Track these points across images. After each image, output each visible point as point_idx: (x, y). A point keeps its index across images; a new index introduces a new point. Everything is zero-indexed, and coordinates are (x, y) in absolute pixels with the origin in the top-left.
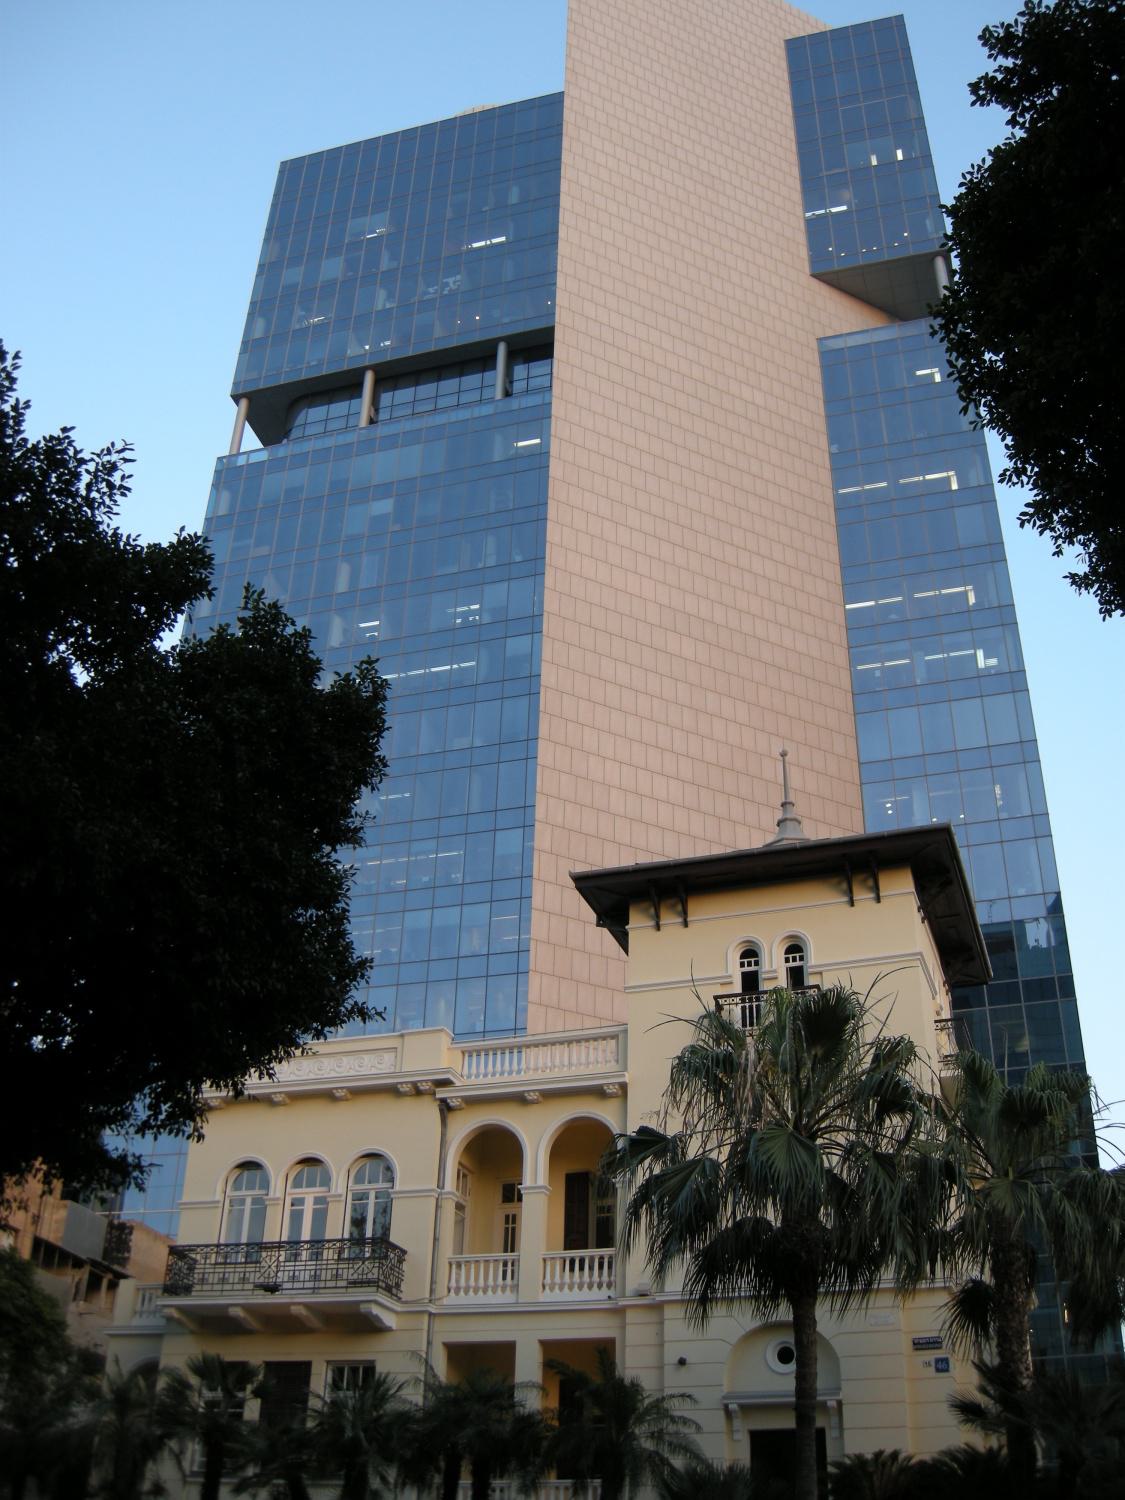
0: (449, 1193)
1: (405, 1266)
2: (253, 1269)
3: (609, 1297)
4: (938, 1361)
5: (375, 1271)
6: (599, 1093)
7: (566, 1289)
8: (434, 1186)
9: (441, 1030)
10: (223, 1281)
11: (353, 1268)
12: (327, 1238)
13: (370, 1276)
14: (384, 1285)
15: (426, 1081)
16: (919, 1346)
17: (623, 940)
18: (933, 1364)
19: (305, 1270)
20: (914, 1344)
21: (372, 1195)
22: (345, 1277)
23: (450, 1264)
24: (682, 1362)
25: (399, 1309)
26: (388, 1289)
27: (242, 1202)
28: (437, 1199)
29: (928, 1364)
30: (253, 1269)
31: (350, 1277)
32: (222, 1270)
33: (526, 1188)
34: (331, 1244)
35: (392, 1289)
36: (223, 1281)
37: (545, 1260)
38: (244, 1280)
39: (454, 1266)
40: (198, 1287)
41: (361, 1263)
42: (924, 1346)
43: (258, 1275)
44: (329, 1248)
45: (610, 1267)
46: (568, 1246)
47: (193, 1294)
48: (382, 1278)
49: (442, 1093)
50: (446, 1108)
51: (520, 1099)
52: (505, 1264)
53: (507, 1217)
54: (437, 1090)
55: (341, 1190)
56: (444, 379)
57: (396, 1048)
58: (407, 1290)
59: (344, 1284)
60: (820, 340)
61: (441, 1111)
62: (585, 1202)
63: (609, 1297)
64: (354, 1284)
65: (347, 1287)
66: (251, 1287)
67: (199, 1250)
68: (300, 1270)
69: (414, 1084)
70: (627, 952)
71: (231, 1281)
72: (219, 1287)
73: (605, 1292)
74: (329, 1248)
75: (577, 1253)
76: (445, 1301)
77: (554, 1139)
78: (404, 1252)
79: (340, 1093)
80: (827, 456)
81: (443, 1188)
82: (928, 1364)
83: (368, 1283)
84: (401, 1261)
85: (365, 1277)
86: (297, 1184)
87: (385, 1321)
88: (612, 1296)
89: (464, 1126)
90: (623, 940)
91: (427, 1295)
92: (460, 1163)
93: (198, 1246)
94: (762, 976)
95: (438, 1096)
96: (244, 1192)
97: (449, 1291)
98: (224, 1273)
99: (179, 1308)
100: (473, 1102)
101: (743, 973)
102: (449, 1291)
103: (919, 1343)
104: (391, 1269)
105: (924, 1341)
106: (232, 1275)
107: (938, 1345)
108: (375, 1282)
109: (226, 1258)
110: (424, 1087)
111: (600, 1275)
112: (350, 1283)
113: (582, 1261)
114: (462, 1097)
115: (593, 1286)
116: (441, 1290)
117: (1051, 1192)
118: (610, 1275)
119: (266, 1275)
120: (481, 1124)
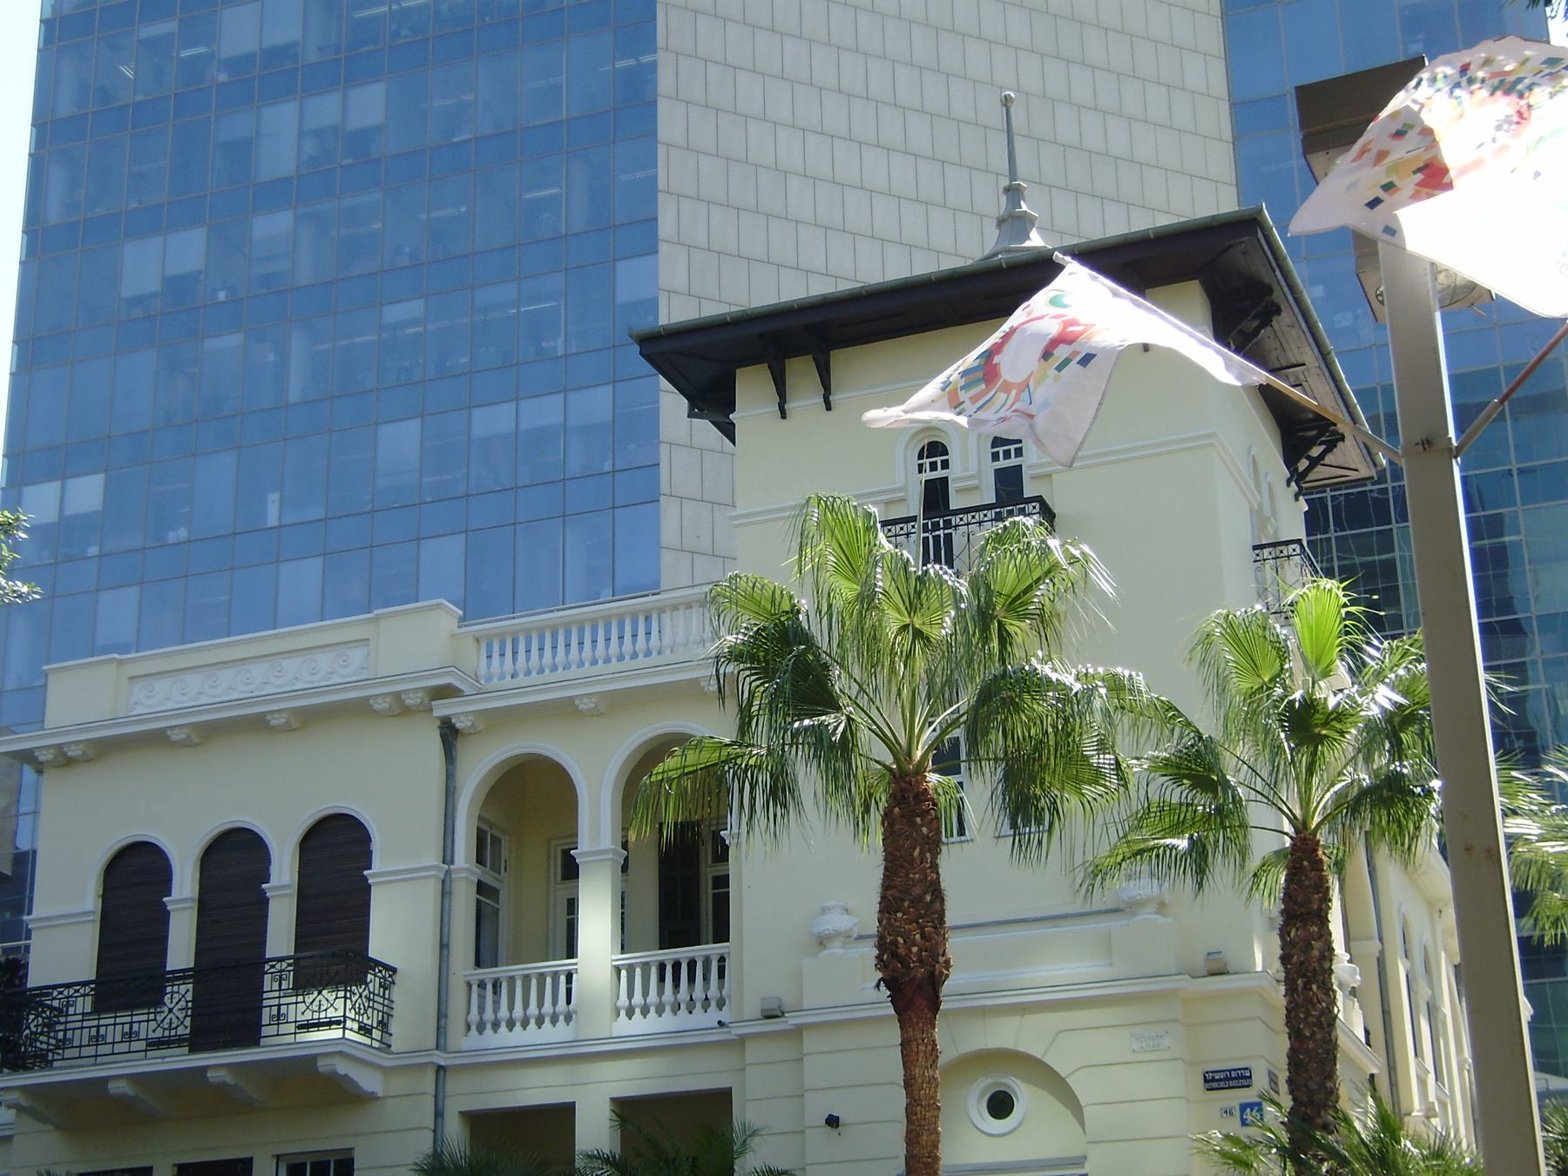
0: (463, 870)
2: (145, 1017)
3: (719, 1022)
4: (1243, 1107)
5: (340, 1003)
7: (532, 1025)
9: (439, 606)
10: (97, 1040)
11: (155, 1020)
13: (331, 1013)
14: (356, 1026)
15: (415, 690)
16: (1215, 1085)
17: (728, 431)
18: (1237, 1112)
19: (115, 1024)
20: (1206, 1081)
22: (143, 1036)
23: (469, 986)
24: (833, 1121)
28: (443, 881)
29: (1228, 1112)
30: (145, 1017)
31: (151, 1035)
32: (95, 1023)
33: (582, 854)
34: (72, 991)
36: (97, 1040)
38: (130, 1036)
39: (475, 988)
40: (272, 1030)
41: (316, 993)
42: (1222, 1084)
43: (153, 1025)
44: (84, 995)
45: (569, 1001)
46: (667, 941)
47: (263, 1041)
48: (351, 1014)
49: (443, 709)
50: (449, 733)
51: (564, 711)
52: (482, 985)
54: (433, 703)
56: (1404, 244)
57: (368, 640)
63: (719, 1022)
65: (146, 1051)
66: (142, 1045)
67: (55, 993)
68: (74, 1029)
69: (397, 696)
70: (734, 444)
71: (76, 1043)
72: (91, 1051)
73: (714, 1015)
74: (84, 995)
75: (683, 953)
77: (624, 781)
78: (394, 970)
79: (176, 736)
81: (452, 862)
82: (1228, 1112)
85: (173, 1033)
87: (361, 1084)
88: (725, 1020)
90: (728, 431)
92: (480, 818)
93: (55, 987)
94: (1026, 474)
95: (438, 713)
97: (468, 1027)
98: (131, 1023)
99: (23, 1089)
101: (997, 471)
102: (468, 1027)
103: (1213, 1080)
104: (369, 1000)
105: (1222, 1076)
106: (78, 1032)
107: (1245, 1082)
108: (338, 1023)
109: (68, 1002)
110: (411, 701)
111: (661, 992)
112: (300, 1027)
113: (692, 964)
115: (528, 1023)
117: (1187, 765)
118: (721, 987)
119: (166, 1026)
120: (509, 754)
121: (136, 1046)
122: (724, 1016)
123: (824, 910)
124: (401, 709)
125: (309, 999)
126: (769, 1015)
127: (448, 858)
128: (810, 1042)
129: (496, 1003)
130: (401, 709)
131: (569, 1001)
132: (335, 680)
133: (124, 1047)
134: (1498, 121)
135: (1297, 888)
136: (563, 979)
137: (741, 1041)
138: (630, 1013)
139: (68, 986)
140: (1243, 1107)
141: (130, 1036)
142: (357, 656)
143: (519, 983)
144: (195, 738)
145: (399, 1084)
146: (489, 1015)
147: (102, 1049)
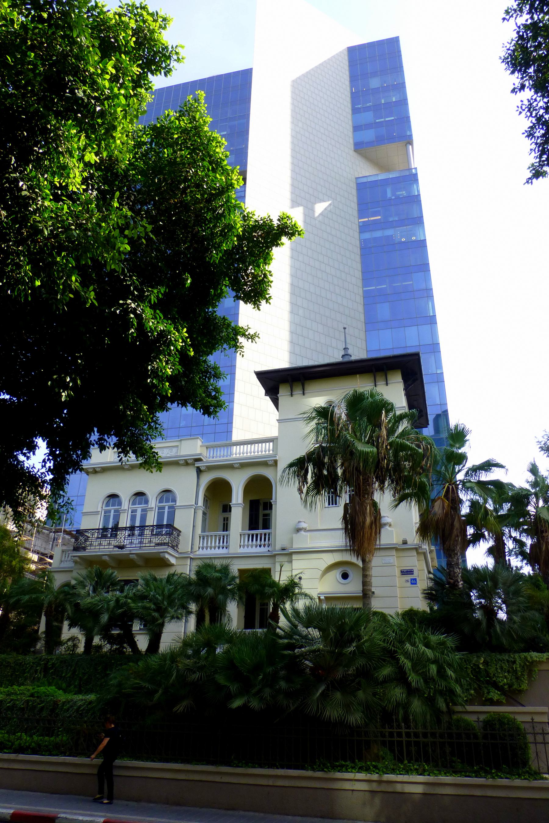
0: (201, 507)
1: (180, 538)
4: (411, 580)
5: (167, 539)
6: (264, 464)
7: (217, 548)
8: (194, 503)
9: (198, 438)
12: (147, 525)
13: (165, 541)
15: (191, 459)
18: (410, 581)
21: (167, 508)
23: (200, 537)
25: (177, 556)
26: (173, 547)
27: (110, 512)
29: (407, 581)
35: (174, 547)
37: (241, 535)
38: (109, 544)
39: (201, 538)
45: (269, 540)
48: (170, 542)
49: (198, 464)
50: (199, 471)
51: (230, 467)
53: (224, 518)
55: (153, 505)
58: (181, 548)
59: (154, 545)
60: (356, 178)
61: (197, 472)
62: (257, 510)
64: (158, 544)
66: (112, 547)
72: (98, 547)
76: (197, 553)
78: (180, 532)
80: (358, 226)
82: (407, 581)
83: (164, 544)
84: (178, 535)
86: (134, 504)
89: (207, 479)
91: (190, 550)
95: (196, 465)
96: (164, 504)
100: (211, 468)
110: (189, 462)
114: (206, 466)
116: (196, 548)
121: (152, 545)
122: (270, 549)
123: (299, 522)
124: (187, 464)
125: (159, 537)
126: (283, 549)
127: (196, 503)
128: (294, 557)
129: (203, 542)
130: (187, 464)
131: (269, 540)
132: (168, 455)
133: (148, 545)
134: (529, 168)
135: (417, 767)
136: (225, 537)
137: (275, 556)
138: (203, 548)
139: (93, 530)
140: (411, 580)
141: (109, 544)
142: (174, 450)
143: (225, 537)
144: (130, 468)
145: (181, 562)
146: (213, 545)
147: (101, 547)
